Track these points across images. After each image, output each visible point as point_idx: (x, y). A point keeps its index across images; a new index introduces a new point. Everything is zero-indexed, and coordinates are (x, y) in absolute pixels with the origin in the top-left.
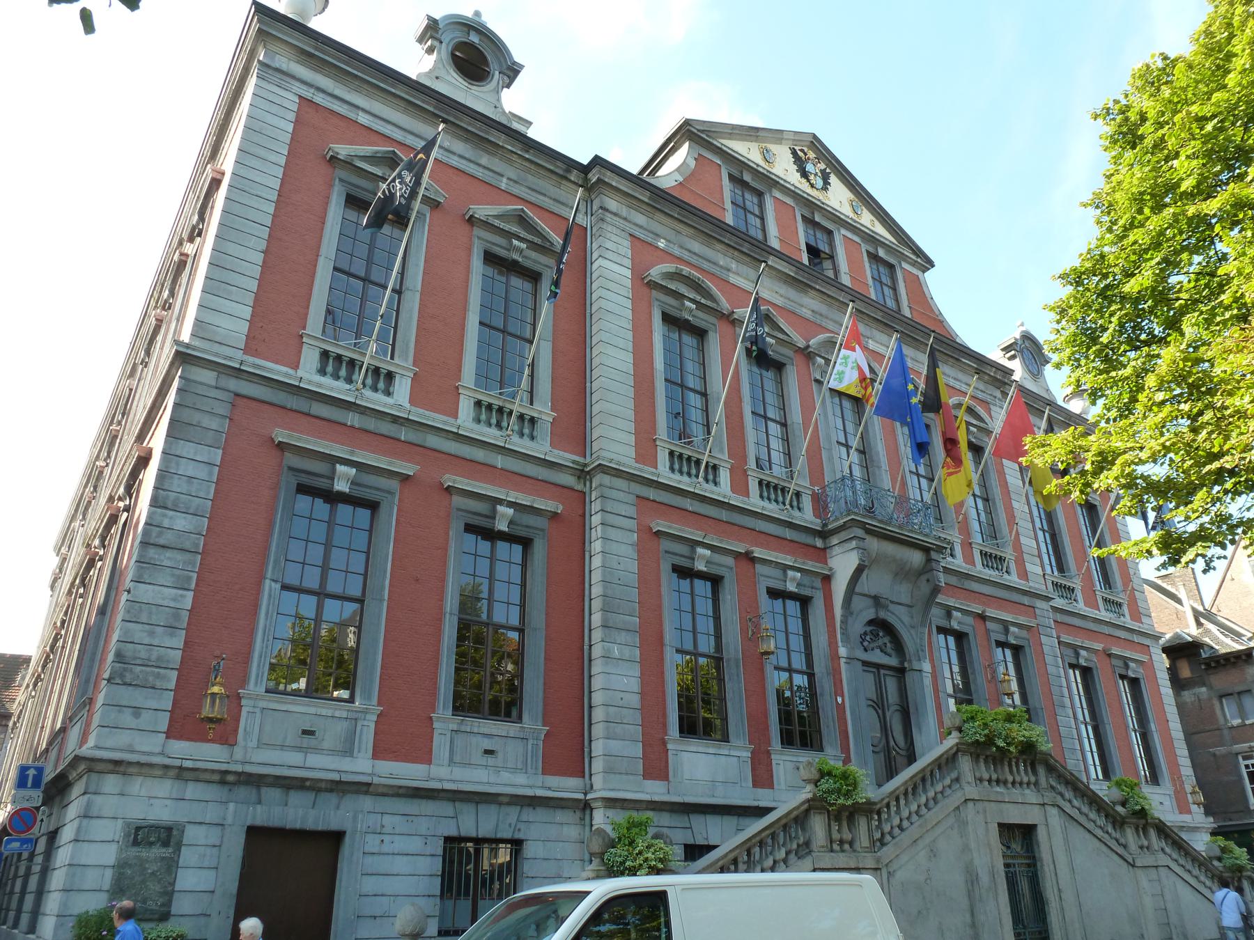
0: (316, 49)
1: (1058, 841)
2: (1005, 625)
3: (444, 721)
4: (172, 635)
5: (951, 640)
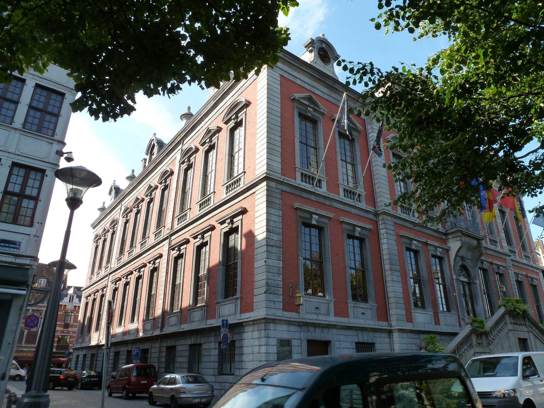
0: (284, 56)
1: (533, 344)
2: (498, 266)
3: (351, 304)
4: (279, 276)
5: (412, 254)
